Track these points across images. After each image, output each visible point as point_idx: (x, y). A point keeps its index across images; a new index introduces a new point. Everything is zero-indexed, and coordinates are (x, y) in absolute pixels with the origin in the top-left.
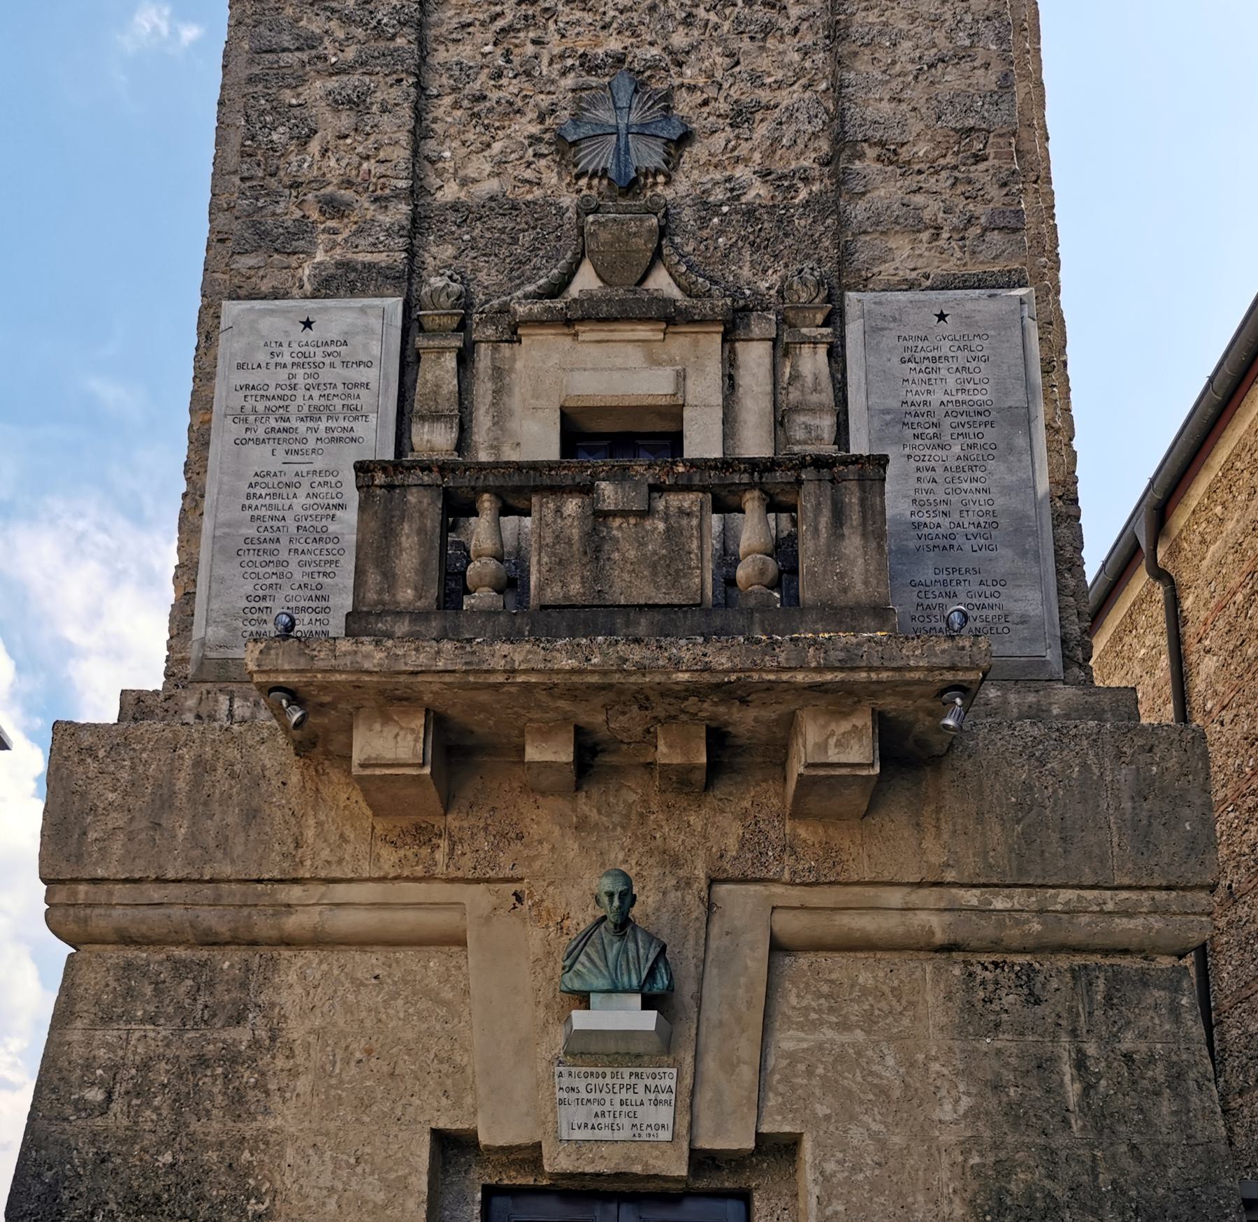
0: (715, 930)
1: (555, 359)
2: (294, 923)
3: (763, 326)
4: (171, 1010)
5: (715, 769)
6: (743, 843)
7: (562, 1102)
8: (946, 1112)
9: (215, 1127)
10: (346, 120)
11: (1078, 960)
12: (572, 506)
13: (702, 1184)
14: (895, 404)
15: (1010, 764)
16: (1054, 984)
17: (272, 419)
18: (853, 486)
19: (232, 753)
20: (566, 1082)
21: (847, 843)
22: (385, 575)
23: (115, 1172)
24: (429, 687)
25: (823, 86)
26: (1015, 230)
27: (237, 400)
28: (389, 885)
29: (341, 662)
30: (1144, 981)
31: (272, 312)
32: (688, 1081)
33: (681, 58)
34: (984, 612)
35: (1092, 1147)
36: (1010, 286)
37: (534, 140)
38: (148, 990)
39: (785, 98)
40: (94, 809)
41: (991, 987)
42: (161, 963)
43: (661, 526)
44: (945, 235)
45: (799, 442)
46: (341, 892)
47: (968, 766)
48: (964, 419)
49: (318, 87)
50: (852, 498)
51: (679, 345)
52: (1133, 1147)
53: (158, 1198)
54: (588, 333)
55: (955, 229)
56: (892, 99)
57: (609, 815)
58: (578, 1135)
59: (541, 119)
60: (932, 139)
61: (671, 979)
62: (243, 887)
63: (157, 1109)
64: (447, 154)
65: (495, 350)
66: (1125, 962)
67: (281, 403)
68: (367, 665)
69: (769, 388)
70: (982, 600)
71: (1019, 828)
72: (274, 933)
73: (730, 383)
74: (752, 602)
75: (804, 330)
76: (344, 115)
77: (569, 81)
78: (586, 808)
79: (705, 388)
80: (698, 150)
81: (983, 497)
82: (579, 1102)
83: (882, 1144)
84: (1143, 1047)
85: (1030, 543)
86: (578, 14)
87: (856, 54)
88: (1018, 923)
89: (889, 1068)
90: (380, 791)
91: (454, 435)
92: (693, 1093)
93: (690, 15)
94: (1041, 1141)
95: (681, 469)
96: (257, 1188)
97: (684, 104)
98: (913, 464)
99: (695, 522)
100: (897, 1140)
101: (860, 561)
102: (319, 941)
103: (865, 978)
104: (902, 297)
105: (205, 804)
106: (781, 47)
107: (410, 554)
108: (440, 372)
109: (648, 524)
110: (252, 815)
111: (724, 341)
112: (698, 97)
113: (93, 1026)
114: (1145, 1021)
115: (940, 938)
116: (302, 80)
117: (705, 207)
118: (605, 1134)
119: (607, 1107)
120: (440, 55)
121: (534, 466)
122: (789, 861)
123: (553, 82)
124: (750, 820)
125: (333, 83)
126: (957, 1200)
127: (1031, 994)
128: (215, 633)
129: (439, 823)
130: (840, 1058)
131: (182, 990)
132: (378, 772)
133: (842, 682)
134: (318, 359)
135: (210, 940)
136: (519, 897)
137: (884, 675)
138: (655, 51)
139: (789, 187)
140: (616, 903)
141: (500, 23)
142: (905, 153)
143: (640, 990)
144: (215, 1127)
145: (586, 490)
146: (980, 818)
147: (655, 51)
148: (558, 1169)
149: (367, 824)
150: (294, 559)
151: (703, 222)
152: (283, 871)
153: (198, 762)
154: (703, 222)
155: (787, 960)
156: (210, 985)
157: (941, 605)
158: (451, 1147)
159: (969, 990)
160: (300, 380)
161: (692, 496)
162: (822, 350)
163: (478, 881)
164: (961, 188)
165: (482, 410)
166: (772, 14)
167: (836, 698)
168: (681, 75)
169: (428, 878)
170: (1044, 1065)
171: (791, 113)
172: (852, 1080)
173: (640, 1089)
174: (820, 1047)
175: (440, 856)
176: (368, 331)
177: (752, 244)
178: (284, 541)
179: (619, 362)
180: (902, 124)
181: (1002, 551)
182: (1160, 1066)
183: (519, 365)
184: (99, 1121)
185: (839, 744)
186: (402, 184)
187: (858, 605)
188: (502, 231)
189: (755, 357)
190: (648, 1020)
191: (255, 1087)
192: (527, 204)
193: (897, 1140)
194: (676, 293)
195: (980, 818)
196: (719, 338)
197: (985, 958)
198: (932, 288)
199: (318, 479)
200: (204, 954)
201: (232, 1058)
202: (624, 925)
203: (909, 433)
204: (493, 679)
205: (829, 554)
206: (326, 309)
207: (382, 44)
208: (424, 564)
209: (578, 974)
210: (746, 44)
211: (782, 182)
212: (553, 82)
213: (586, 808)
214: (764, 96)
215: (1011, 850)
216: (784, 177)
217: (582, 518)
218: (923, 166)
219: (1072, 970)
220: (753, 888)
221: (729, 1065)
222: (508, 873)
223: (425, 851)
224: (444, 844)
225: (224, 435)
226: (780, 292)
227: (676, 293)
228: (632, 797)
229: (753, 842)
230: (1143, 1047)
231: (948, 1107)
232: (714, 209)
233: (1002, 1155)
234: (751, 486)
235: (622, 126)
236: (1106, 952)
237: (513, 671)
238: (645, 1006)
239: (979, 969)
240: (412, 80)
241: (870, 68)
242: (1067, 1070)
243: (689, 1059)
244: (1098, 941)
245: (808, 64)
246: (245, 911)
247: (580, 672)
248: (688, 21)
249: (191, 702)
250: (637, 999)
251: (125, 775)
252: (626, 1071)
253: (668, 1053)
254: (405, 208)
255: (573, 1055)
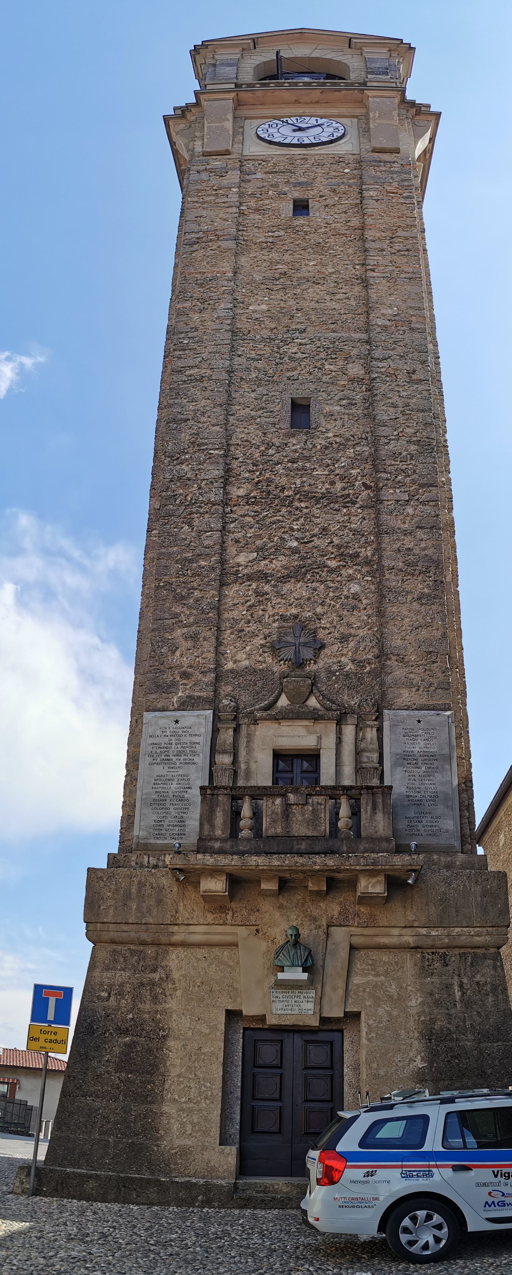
0: (329, 943)
1: (272, 731)
2: (175, 939)
3: (352, 720)
4: (130, 967)
5: (328, 891)
6: (340, 913)
7: (273, 1001)
8: (413, 1003)
9: (147, 1006)
10: (190, 644)
11: (463, 951)
12: (278, 801)
13: (325, 1028)
14: (401, 752)
15: (439, 885)
16: (453, 959)
17: (163, 756)
18: (380, 796)
19: (152, 880)
20: (275, 994)
21: (378, 913)
22: (211, 826)
23: (112, 1020)
24: (229, 869)
25: (376, 629)
26: (447, 689)
27: (150, 749)
28: (210, 926)
29: (199, 862)
30: (485, 957)
31: (163, 717)
32: (319, 994)
33: (320, 617)
34: (432, 828)
35: (464, 1013)
36: (446, 710)
37: (263, 646)
38: (122, 960)
39: (361, 633)
40: (103, 898)
41: (431, 961)
42: (126, 951)
43: (311, 808)
44: (421, 690)
45: (365, 763)
46: (192, 929)
47: (423, 886)
48: (427, 758)
49: (179, 632)
50: (380, 800)
51: (320, 727)
52: (478, 1013)
53: (128, 1029)
54: (284, 723)
55: (425, 687)
56: (401, 639)
57: (291, 903)
58: (279, 1012)
59: (265, 638)
60: (417, 654)
61: (313, 961)
62: (156, 926)
63: (126, 1000)
64: (228, 651)
65: (248, 727)
66: (479, 951)
67: (165, 750)
68: (208, 863)
69: (354, 741)
70: (432, 824)
71: (441, 908)
72: (167, 942)
73: (339, 741)
74: (343, 836)
75: (368, 723)
76: (189, 642)
77: (276, 625)
78: (282, 901)
79: (329, 742)
80: (327, 651)
81: (433, 786)
82: (280, 1001)
83: (390, 1014)
84: (483, 979)
85: (450, 803)
86: (279, 600)
87: (388, 622)
88: (440, 940)
89: (393, 989)
90: (209, 899)
91: (232, 759)
92: (321, 998)
93: (323, 602)
94: (446, 1012)
95: (318, 789)
96: (163, 1027)
97: (321, 634)
98: (407, 774)
99: (323, 807)
100: (395, 1013)
101: (382, 822)
102: (184, 945)
103: (385, 959)
104: (404, 713)
105: (143, 897)
106: (359, 614)
107: (220, 818)
108: (227, 736)
109: (306, 808)
110: (159, 902)
111: (337, 724)
112: (327, 631)
113: (102, 971)
114: (484, 971)
115: (412, 945)
116: (173, 630)
117: (331, 673)
118: (290, 1012)
119: (290, 1003)
120: (226, 615)
121: (264, 788)
122: (357, 919)
123: (270, 625)
124: (343, 905)
125: (185, 630)
126: (416, 1032)
127: (445, 963)
128: (142, 834)
129: (228, 906)
130: (376, 986)
131: (134, 960)
132: (209, 894)
133: (372, 869)
134: (180, 733)
135: (144, 943)
136: (257, 931)
137: (387, 867)
138: (310, 614)
139: (362, 666)
140: (293, 938)
141: (249, 603)
142: (406, 659)
143: (302, 966)
144: (147, 1006)
145: (284, 795)
146: (427, 905)
147: (310, 614)
148: (272, 1023)
149: (202, 905)
150: (172, 807)
151: (329, 679)
152: (171, 921)
153: (140, 883)
154: (329, 679)
155: (356, 952)
156: (144, 958)
157: (416, 825)
158: (232, 1016)
159: (423, 962)
160: (173, 741)
161: (322, 797)
162: (375, 730)
163: (242, 925)
164: (427, 673)
165: (242, 749)
166: (356, 602)
167: (372, 873)
168: (320, 623)
169: (225, 924)
170: (448, 987)
171: (363, 639)
172: (379, 994)
173: (302, 997)
174: (368, 982)
175: (228, 917)
176: (200, 724)
177: (348, 687)
178: (168, 800)
179: (296, 733)
180: (406, 649)
181: (439, 806)
182: (489, 986)
183: (257, 733)
184: (106, 1003)
185: (372, 886)
186: (212, 666)
187: (381, 838)
188: (250, 680)
189: (349, 731)
190: (305, 976)
191: (161, 993)
192: (260, 670)
193: (395, 1013)
194: (318, 706)
195: (427, 905)
196: (335, 725)
197: (429, 951)
198: (417, 709)
199: (180, 778)
200: (141, 948)
201: (152, 984)
202: (296, 944)
203: (406, 762)
204: (251, 868)
205: (371, 819)
206: (184, 716)
207: (203, 616)
208: (225, 822)
209: (280, 960)
210: (345, 612)
211: (360, 664)
212: (270, 625)
213: (282, 901)
214: (353, 631)
215: (438, 915)
216: (360, 662)
217: (282, 805)
218: (414, 664)
219: (460, 954)
220: (343, 928)
221: (334, 989)
222: (254, 923)
223: (223, 915)
224: (230, 913)
225: (144, 763)
226: (359, 706)
227: (318, 706)
228: (299, 897)
229: (344, 912)
230: (483, 979)
231: (414, 1002)
232: (333, 673)
233: (432, 1017)
234: (344, 794)
235: (297, 643)
236: (472, 948)
237: (258, 865)
238: (303, 971)
239: (427, 955)
240: (215, 628)
241: (393, 627)
242: (456, 988)
243: (320, 987)
244: (469, 945)
245: (370, 621)
246: (157, 934)
247: (281, 866)
248: (323, 604)
249: (134, 858)
250: (301, 969)
251: (113, 887)
252: (297, 991)
253: (312, 985)
254: (213, 675)
255: (277, 986)
